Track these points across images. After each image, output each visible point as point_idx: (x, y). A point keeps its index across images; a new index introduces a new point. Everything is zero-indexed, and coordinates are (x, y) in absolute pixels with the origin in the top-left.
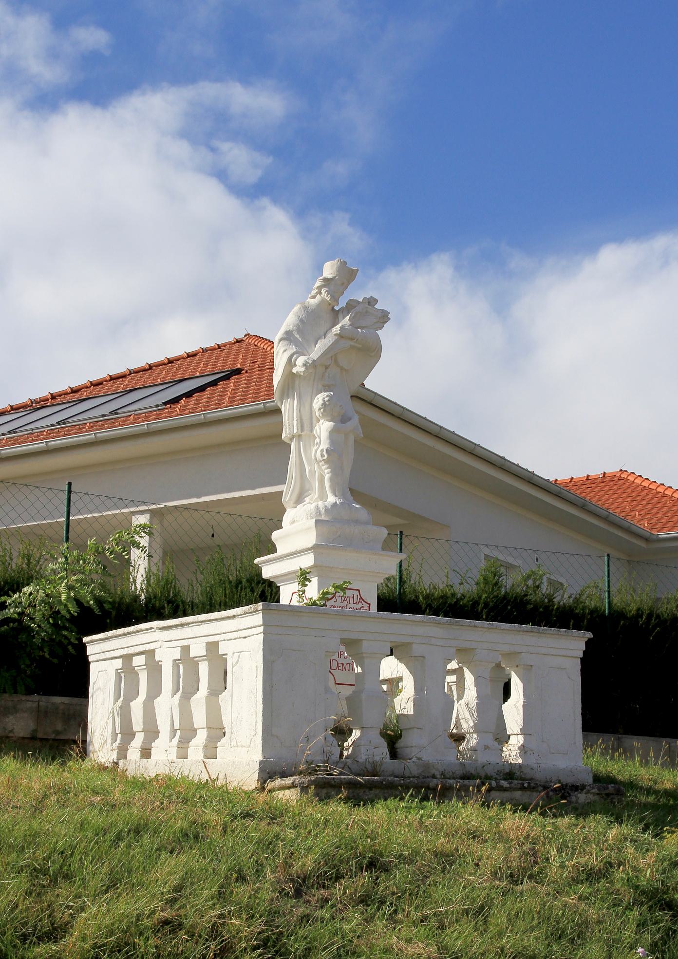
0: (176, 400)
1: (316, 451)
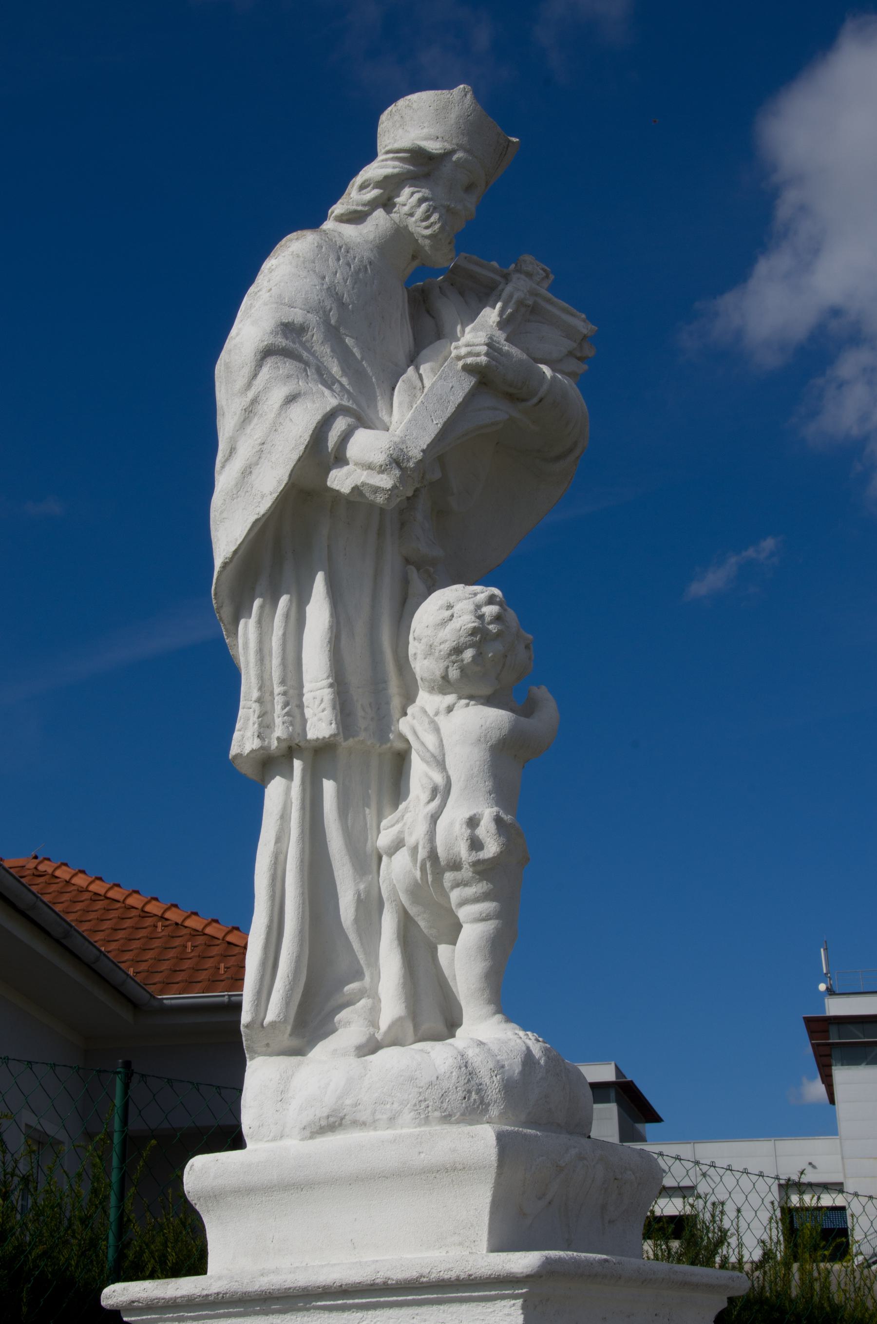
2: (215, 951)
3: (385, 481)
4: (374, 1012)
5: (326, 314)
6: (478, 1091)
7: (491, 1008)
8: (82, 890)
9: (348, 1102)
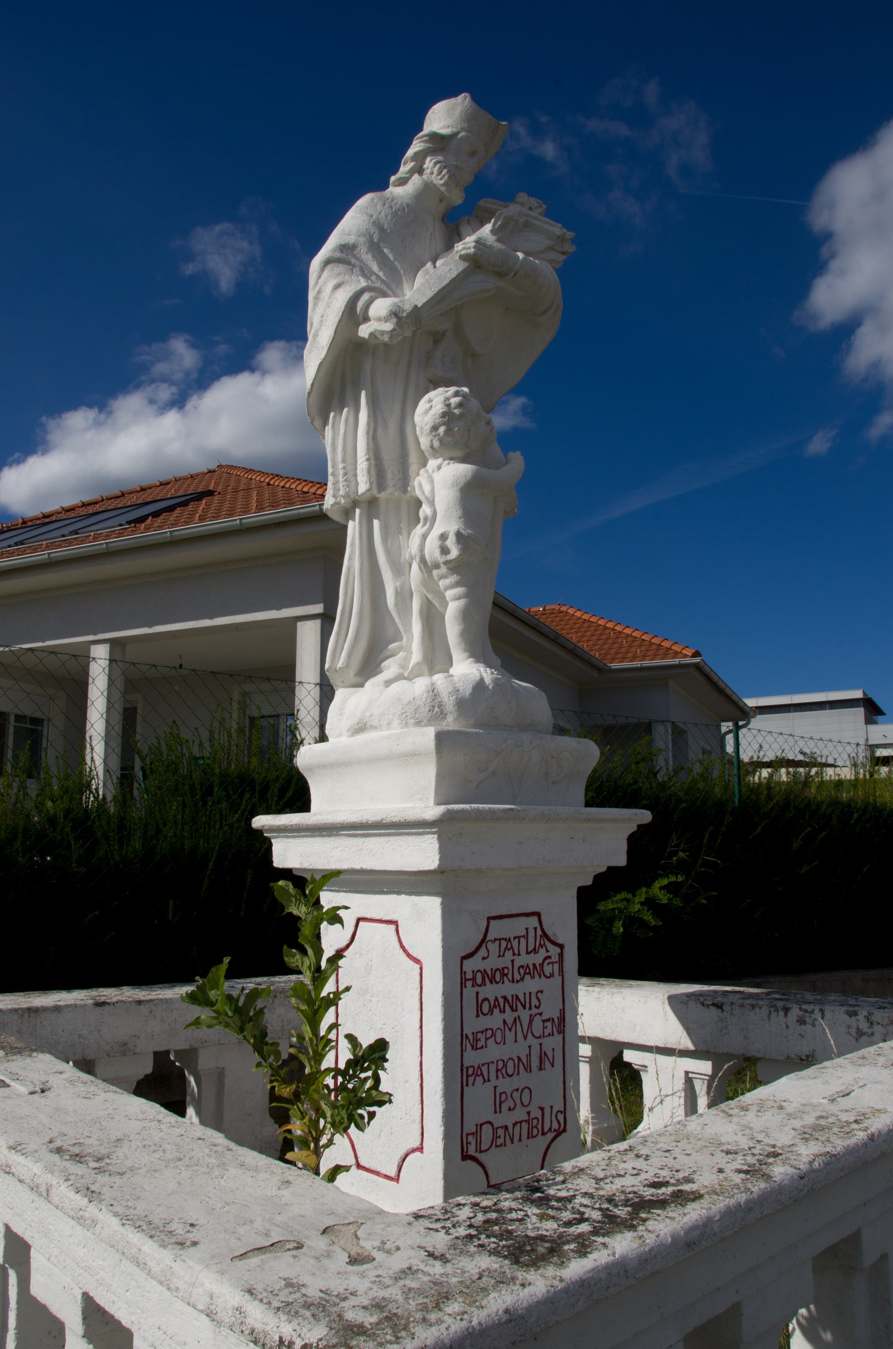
0: (142, 520)
1: (424, 537)
2: (636, 643)
3: (388, 327)
4: (407, 658)
5: (371, 237)
6: (440, 706)
7: (467, 654)
8: (578, 618)
9: (367, 714)
